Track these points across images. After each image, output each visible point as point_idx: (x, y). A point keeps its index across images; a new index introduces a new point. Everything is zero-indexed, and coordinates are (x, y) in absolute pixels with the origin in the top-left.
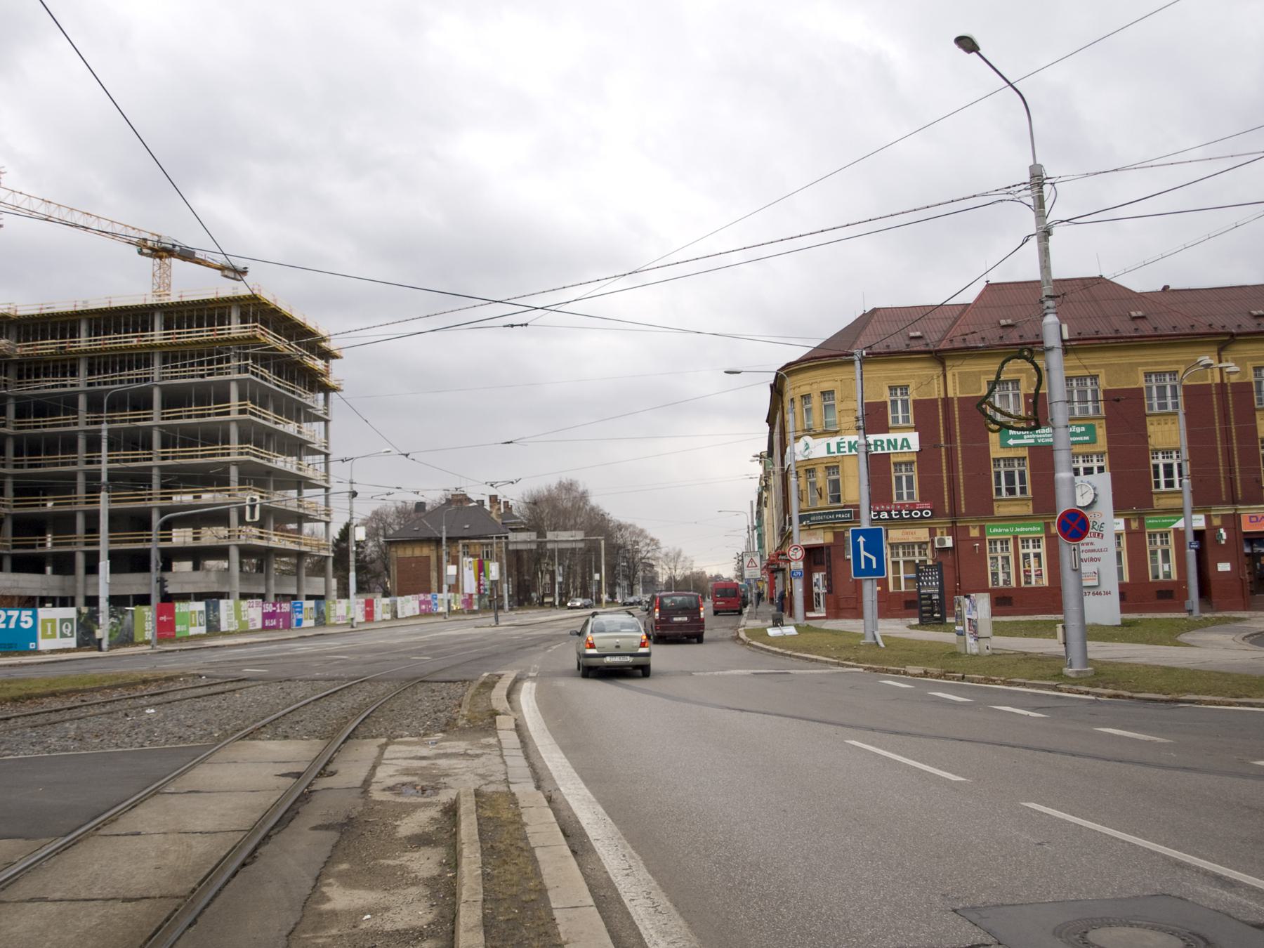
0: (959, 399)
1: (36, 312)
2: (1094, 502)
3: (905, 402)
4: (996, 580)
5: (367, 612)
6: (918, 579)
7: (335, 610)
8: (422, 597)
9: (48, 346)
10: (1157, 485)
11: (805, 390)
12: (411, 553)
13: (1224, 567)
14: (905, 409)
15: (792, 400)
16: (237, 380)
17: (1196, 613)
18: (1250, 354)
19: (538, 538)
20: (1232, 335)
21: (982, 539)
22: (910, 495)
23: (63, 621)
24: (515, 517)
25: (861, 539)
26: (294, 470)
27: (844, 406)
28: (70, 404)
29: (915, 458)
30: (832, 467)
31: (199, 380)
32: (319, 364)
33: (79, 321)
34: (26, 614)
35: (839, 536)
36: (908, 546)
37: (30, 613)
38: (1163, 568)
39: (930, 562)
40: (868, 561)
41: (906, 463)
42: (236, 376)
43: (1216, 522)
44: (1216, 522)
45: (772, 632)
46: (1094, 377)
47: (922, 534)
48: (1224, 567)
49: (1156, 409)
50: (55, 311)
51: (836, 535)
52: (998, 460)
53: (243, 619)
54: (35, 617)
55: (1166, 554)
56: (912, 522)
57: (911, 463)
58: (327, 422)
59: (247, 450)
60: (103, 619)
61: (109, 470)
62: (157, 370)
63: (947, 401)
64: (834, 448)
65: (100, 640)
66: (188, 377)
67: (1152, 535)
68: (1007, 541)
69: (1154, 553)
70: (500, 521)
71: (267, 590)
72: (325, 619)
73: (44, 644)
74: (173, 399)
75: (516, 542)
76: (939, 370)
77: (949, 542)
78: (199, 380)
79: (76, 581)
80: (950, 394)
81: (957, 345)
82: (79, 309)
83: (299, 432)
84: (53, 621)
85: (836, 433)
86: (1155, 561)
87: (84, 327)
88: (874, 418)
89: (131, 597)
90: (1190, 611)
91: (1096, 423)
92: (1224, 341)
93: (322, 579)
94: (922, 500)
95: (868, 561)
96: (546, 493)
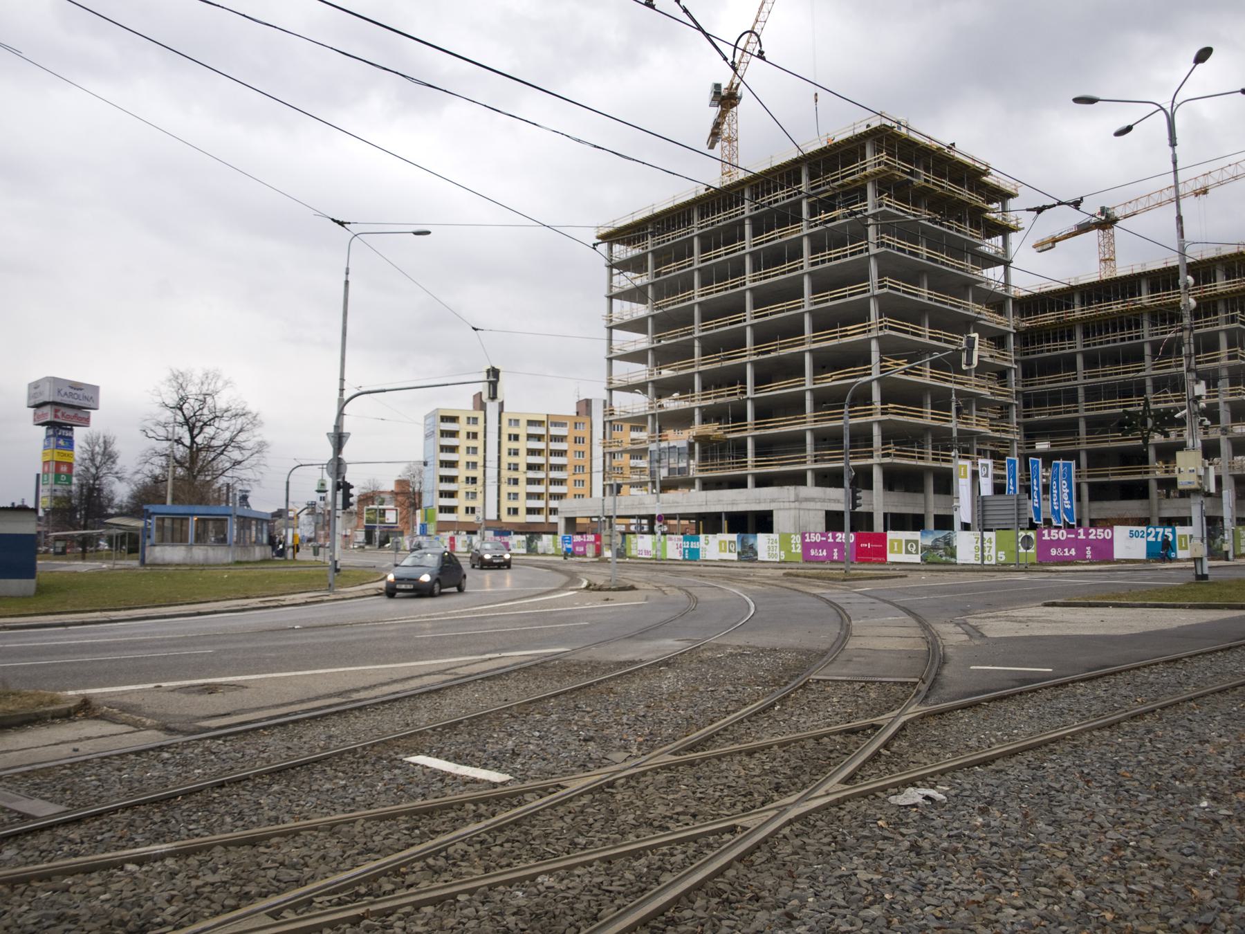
9: (1049, 318)
16: (1226, 331)
28: (1068, 363)
33: (1073, 294)
34: (1168, 531)
37: (1170, 530)
42: (1224, 327)
61: (871, 404)
62: (1146, 329)
65: (1227, 552)
84: (900, 542)
87: (1077, 300)
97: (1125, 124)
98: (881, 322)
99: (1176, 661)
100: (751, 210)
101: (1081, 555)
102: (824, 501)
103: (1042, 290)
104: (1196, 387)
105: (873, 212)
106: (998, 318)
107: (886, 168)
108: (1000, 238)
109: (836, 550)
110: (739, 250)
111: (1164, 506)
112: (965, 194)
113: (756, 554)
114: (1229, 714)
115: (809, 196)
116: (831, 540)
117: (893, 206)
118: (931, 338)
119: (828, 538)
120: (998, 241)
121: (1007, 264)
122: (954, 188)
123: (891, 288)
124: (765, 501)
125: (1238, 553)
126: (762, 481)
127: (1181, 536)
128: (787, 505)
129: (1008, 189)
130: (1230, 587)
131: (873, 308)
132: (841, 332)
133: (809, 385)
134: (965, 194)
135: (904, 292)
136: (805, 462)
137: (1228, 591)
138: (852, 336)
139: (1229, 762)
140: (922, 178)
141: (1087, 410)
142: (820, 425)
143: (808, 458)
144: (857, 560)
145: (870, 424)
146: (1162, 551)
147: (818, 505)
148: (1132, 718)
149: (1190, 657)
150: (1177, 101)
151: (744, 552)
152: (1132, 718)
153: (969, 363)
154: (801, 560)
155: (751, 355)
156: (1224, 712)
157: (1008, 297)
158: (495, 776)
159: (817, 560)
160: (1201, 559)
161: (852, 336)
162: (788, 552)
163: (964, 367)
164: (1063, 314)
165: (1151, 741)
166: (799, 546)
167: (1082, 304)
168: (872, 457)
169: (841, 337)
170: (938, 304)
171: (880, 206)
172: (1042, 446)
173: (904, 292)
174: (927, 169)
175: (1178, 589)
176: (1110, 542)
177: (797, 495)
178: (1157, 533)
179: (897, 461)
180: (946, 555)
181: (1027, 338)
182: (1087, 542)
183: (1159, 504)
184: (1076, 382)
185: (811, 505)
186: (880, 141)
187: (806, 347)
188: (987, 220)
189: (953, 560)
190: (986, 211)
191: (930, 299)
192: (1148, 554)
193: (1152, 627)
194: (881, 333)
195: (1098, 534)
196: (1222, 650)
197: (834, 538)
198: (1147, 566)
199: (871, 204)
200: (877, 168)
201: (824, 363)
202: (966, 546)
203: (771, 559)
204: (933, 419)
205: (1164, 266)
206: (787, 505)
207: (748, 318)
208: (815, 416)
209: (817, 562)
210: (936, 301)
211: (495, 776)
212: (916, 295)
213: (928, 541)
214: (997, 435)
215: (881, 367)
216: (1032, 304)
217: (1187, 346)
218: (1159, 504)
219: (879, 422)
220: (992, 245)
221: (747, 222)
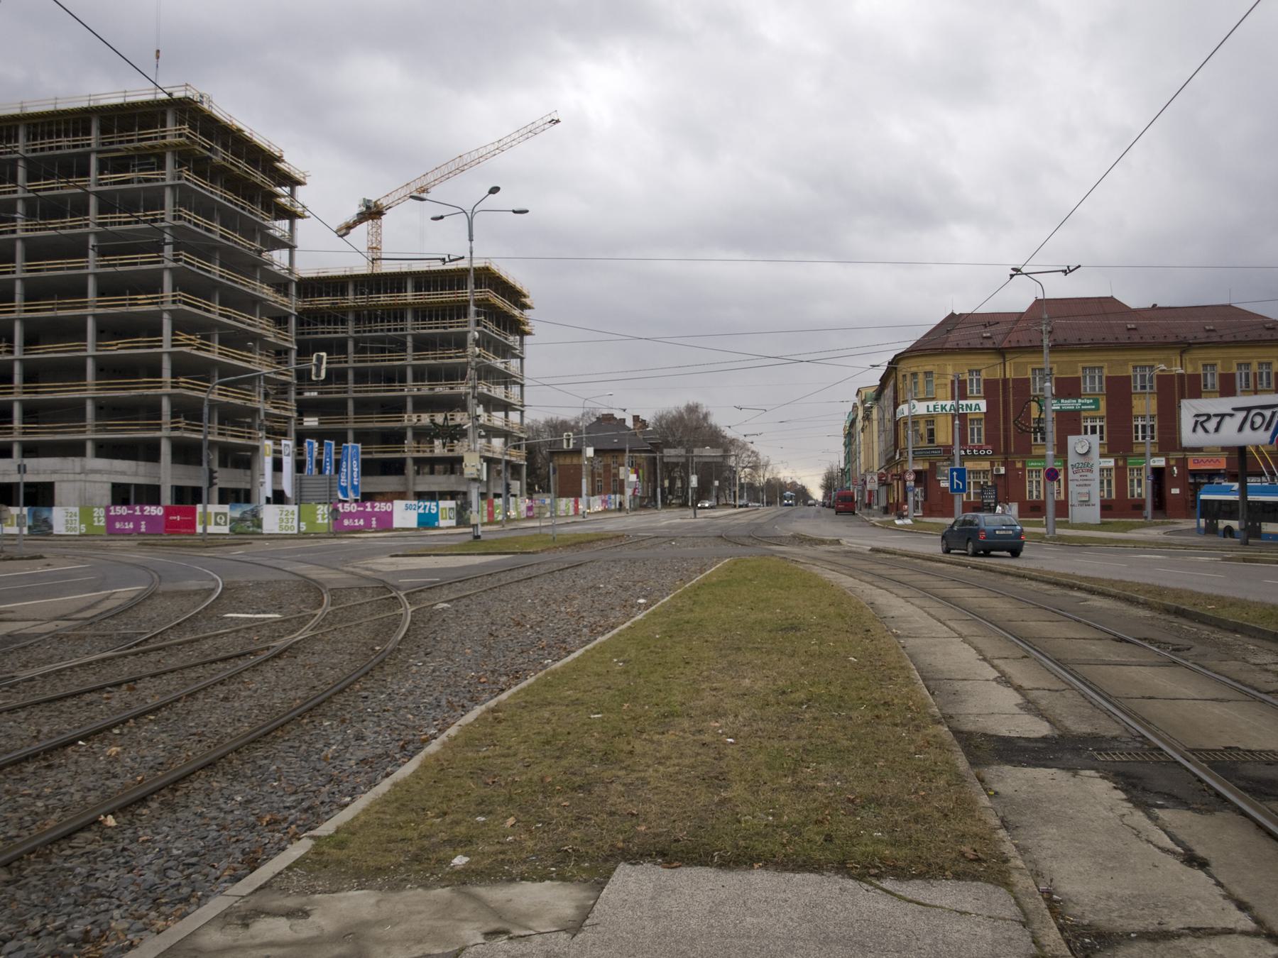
0: (1014, 380)
1: (314, 275)
2: (1088, 451)
3: (978, 380)
4: (1031, 495)
6: (982, 493)
8: (603, 497)
9: (324, 302)
10: (1137, 438)
11: (914, 369)
13: (1175, 491)
14: (978, 385)
15: (904, 376)
17: (1149, 518)
18: (1201, 356)
20: (1190, 344)
21: (1023, 469)
22: (979, 440)
23: (450, 509)
24: (630, 430)
25: (955, 473)
26: (502, 397)
27: (939, 382)
29: (983, 416)
30: (930, 420)
31: (443, 330)
32: (516, 312)
35: (933, 465)
36: (976, 473)
38: (1137, 490)
39: (990, 484)
40: (958, 485)
41: (977, 420)
43: (1172, 462)
44: (1172, 462)
45: (897, 522)
46: (1101, 368)
47: (986, 465)
48: (1175, 491)
49: (1139, 390)
50: (330, 274)
51: (930, 464)
52: (1032, 471)
54: (437, 506)
55: (1139, 482)
56: (979, 458)
57: (981, 420)
58: (522, 359)
62: (409, 322)
63: (1005, 381)
64: (931, 409)
66: (433, 329)
67: (1131, 470)
68: (1039, 471)
69: (1132, 481)
73: (443, 523)
74: (422, 344)
76: (1001, 361)
77: (1002, 471)
78: (443, 330)
79: (406, 480)
80: (1008, 376)
81: (1014, 345)
82: (348, 273)
85: (933, 399)
86: (1132, 486)
87: (351, 288)
88: (960, 391)
90: (1146, 518)
91: (1100, 397)
92: (1184, 347)
93: (518, 483)
94: (987, 443)
95: (958, 485)
96: (674, 413)
97: (439, 215)
98: (174, 296)
100: (27, 151)
101: (368, 524)
102: (110, 473)
103: (321, 275)
105: (171, 183)
106: (280, 299)
107: (187, 142)
108: (287, 222)
109: (143, 523)
110: (9, 192)
111: (417, 481)
112: (258, 177)
113: (51, 527)
115: (99, 152)
116: (138, 513)
117: (191, 180)
118: (221, 315)
119: (135, 511)
120: (284, 224)
121: (292, 248)
122: (249, 169)
123: (186, 262)
124: (45, 472)
126: (30, 450)
127: (443, 509)
128: (71, 477)
129: (297, 176)
131: (167, 280)
132: (130, 299)
133: (91, 351)
134: (258, 177)
135: (198, 267)
136: (84, 432)
138: (142, 305)
140: (220, 156)
141: (355, 392)
142: (102, 394)
143: (88, 428)
144: (166, 532)
145: (159, 397)
146: (427, 522)
147: (105, 478)
150: (476, 210)
151: (35, 526)
153: (318, 375)
154: (104, 532)
155: (20, 311)
157: (292, 281)
158: (277, 616)
159: (123, 532)
161: (142, 305)
162: (90, 525)
163: (314, 378)
164: (338, 299)
166: (103, 519)
167: (356, 294)
168: (160, 430)
169: (130, 305)
170: (229, 283)
171: (179, 178)
172: (311, 422)
173: (198, 267)
174: (225, 147)
176: (390, 514)
177: (83, 468)
178: (425, 506)
179: (187, 435)
180: (254, 526)
181: (306, 318)
182: (373, 514)
183: (414, 480)
184: (346, 365)
185: (97, 477)
186: (183, 111)
187: (89, 311)
188: (277, 204)
189: (259, 530)
190: (278, 196)
191: (221, 276)
192: (419, 523)
193: (461, 564)
194: (173, 307)
195: (381, 507)
197: (142, 511)
198: (418, 533)
199: (169, 173)
200: (178, 139)
201: (109, 330)
202: (273, 519)
203: (69, 533)
204: (220, 394)
205: (427, 269)
206: (71, 477)
207: (18, 269)
208: (97, 385)
209: (124, 534)
210: (228, 279)
211: (277, 616)
212: (209, 272)
213: (237, 514)
214: (276, 412)
215: (173, 340)
216: (311, 287)
218: (414, 480)
219: (169, 395)
220: (280, 227)
221: (21, 163)
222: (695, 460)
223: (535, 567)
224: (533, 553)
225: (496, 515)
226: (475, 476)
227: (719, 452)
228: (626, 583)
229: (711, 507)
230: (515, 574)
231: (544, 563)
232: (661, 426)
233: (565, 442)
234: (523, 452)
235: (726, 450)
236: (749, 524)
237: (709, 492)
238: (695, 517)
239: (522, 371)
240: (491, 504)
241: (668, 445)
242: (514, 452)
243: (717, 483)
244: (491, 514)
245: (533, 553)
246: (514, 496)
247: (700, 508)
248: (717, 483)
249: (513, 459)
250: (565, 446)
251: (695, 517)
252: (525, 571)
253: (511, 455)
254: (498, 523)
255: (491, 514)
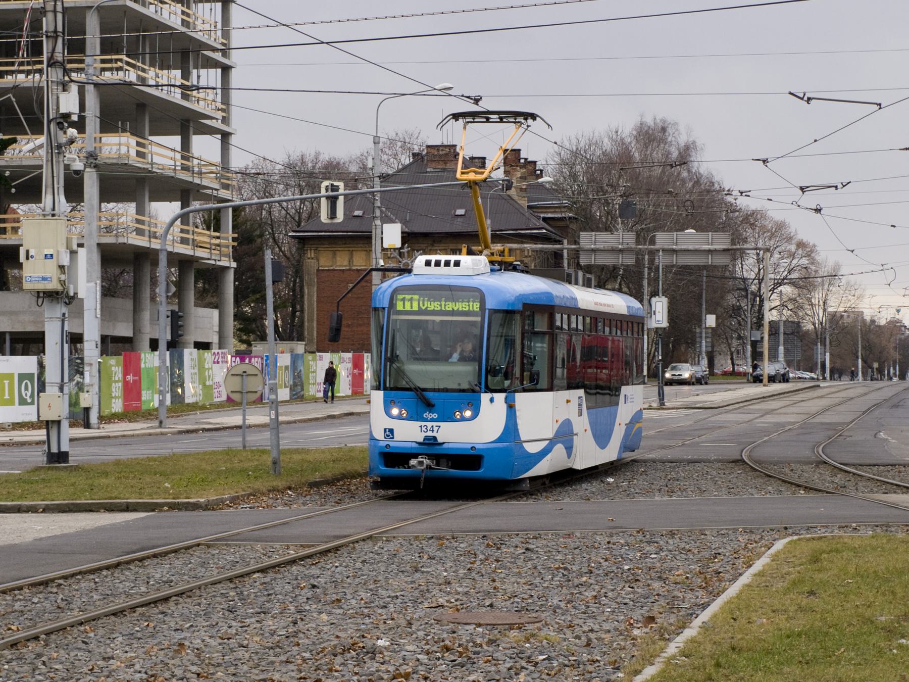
5: (354, 376)
7: (315, 372)
12: (346, 263)
19: (638, 242)
23: (22, 377)
53: (207, 383)
59: (120, 64)
60: (91, 376)
65: (87, 410)
70: (524, 203)
71: (137, 329)
72: (302, 389)
75: (594, 251)
83: (185, 23)
89: (8, 337)
93: (215, 313)
96: (607, 145)
99: (45, 583)
104: (63, 97)
114: (132, 634)
125: (106, 412)
130: (106, 474)
137: (104, 481)
139: (140, 672)
148: (12, 646)
149: (65, 578)
152: (12, 646)
156: (124, 633)
160: (59, 423)
165: (44, 663)
175: (20, 480)
196: (108, 568)
217: (50, 16)
222: (662, 260)
223: (196, 557)
224: (207, 507)
225: (145, 395)
226: (53, 285)
227: (720, 242)
228: (464, 632)
229: (698, 381)
230: (123, 581)
231: (225, 541)
232: (574, 176)
233: (324, 204)
234: (228, 235)
235: (737, 238)
236: (806, 427)
237: (692, 342)
238: (662, 406)
239: (226, 34)
240: (131, 367)
241: (591, 225)
242: (204, 236)
243: (711, 320)
244: (132, 391)
245: (207, 507)
246: (203, 346)
247: (670, 383)
248: (711, 320)
249: (200, 253)
250: (324, 217)
251: (662, 406)
252: (158, 571)
253: (197, 245)
254: (149, 415)
255: (132, 391)
